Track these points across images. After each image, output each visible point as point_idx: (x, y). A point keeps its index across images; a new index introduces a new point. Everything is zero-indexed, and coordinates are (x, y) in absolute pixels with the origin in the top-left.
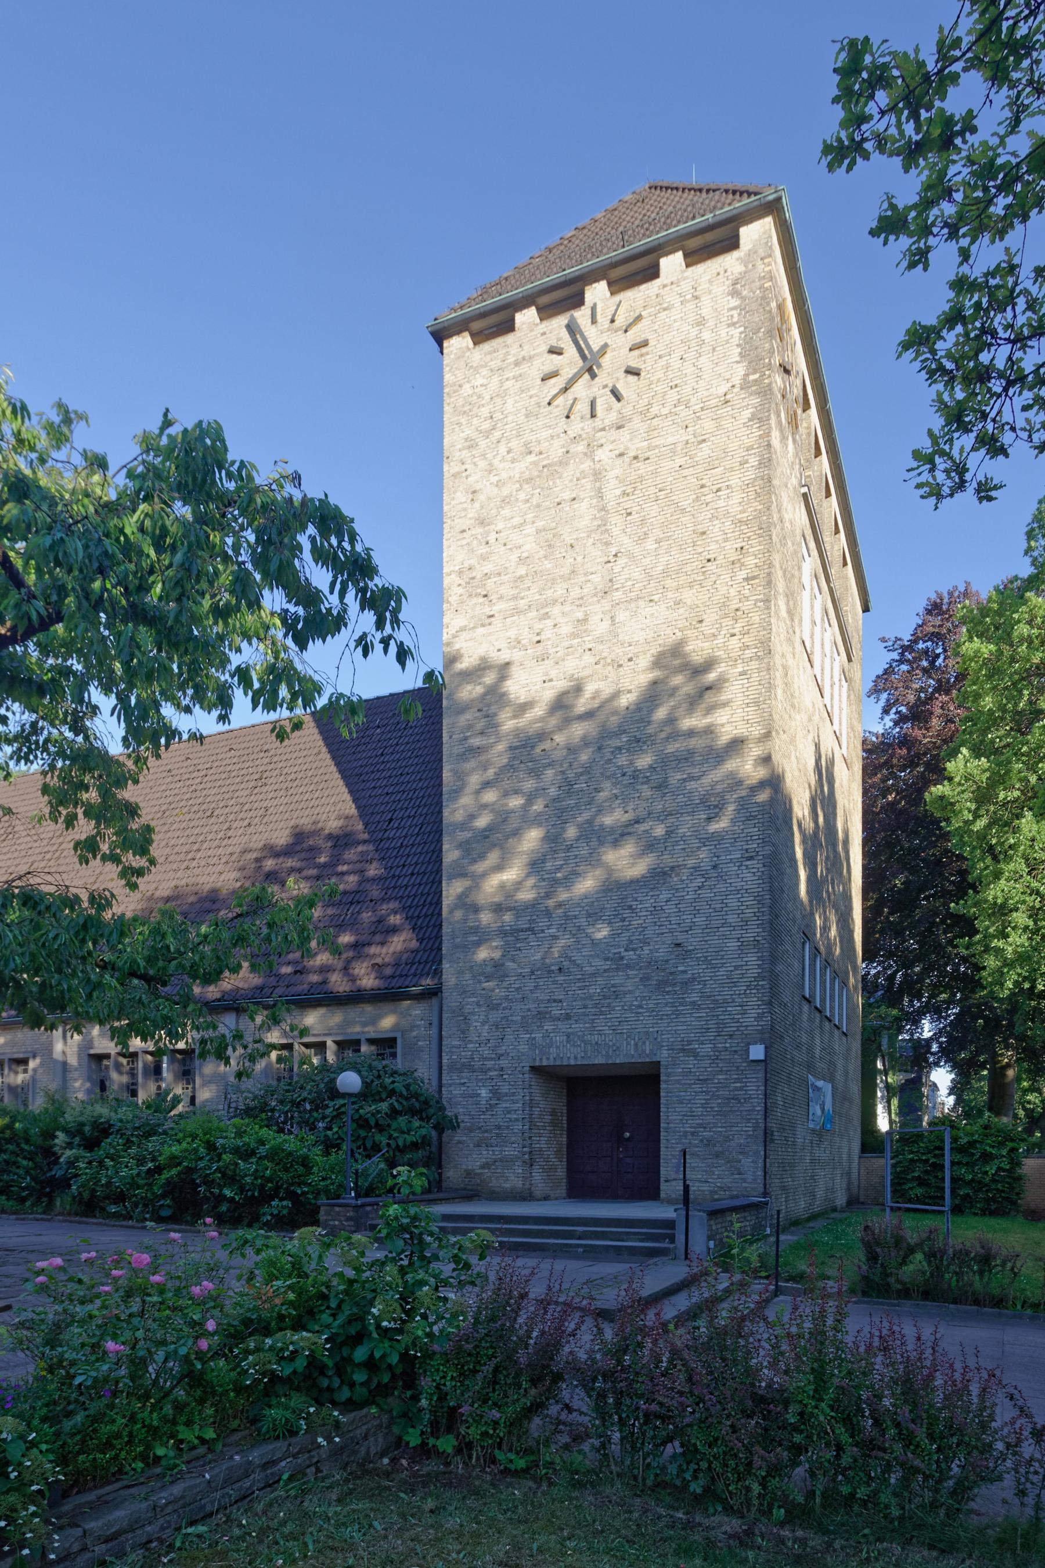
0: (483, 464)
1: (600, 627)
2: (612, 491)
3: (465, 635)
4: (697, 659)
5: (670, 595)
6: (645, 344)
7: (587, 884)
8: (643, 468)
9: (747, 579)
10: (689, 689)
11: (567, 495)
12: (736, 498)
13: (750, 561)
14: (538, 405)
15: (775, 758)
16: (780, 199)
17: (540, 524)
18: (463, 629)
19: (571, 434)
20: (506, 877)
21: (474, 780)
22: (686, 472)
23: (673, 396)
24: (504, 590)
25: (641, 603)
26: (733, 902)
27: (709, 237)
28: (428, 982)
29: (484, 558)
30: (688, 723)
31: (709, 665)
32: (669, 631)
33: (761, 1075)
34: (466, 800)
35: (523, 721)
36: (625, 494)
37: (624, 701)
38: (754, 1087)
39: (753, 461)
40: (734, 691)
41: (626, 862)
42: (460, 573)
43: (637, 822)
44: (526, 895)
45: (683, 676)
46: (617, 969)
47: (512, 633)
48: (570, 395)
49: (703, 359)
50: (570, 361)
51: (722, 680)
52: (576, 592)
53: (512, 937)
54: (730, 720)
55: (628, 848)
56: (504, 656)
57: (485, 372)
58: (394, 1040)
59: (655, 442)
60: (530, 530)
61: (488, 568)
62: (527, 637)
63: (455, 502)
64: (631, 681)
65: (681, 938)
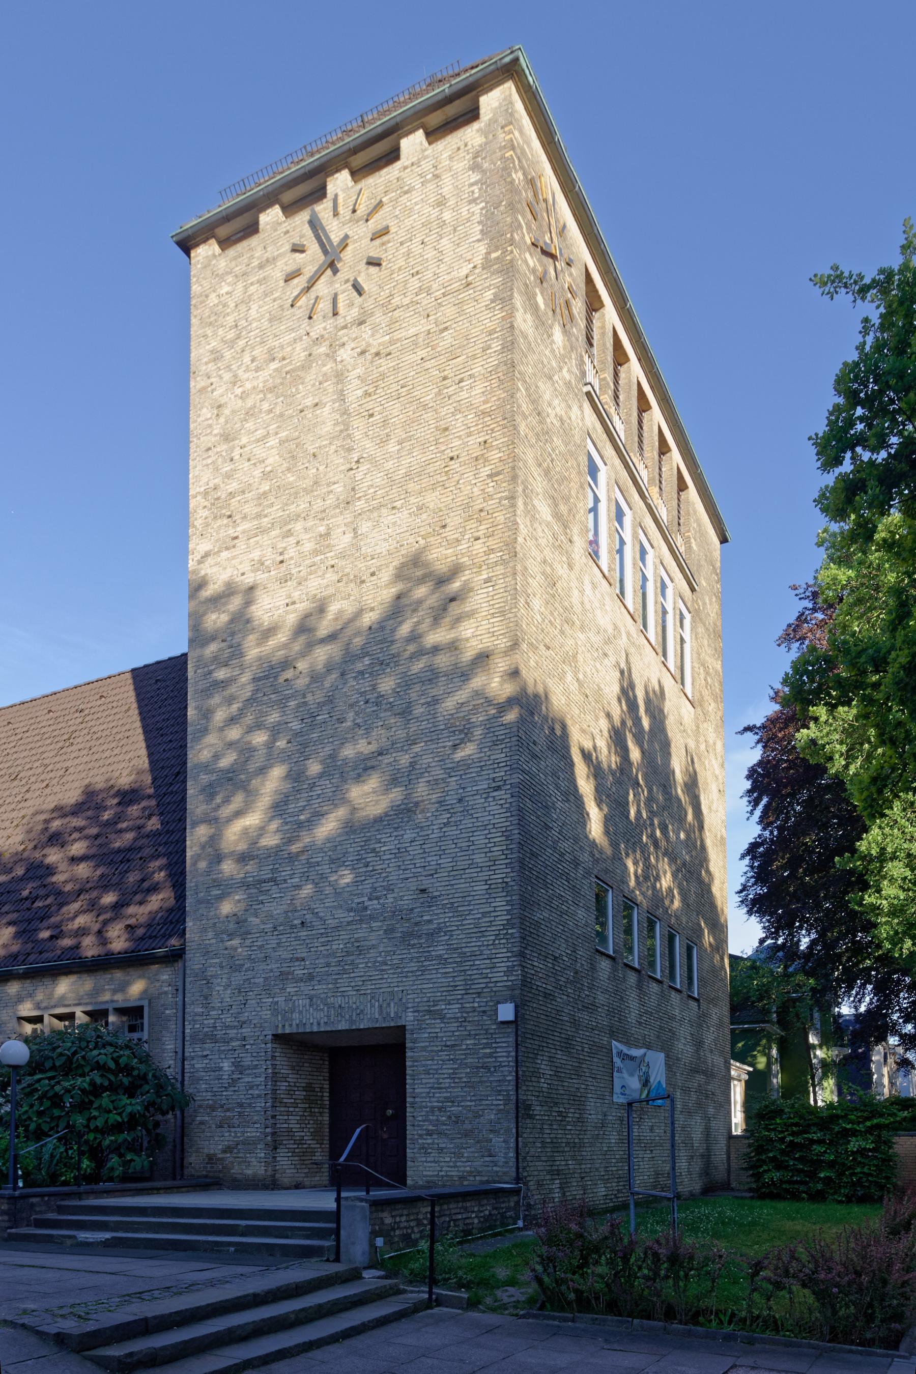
0: (227, 376)
1: (342, 540)
2: (354, 392)
3: (210, 560)
4: (441, 567)
6: (385, 231)
8: (385, 364)
9: (490, 476)
10: (433, 601)
11: (309, 402)
13: (495, 455)
15: (524, 672)
18: (207, 555)
22: (428, 365)
23: (414, 283)
25: (384, 511)
28: (174, 942)
29: (228, 476)
30: (434, 638)
31: (456, 571)
32: (412, 540)
33: (512, 1039)
34: (211, 739)
36: (367, 394)
38: (505, 1053)
39: (496, 346)
41: (369, 797)
44: (270, 841)
45: (431, 586)
47: (256, 555)
48: (312, 294)
49: (444, 241)
50: (314, 255)
53: (255, 888)
54: (476, 632)
55: (373, 783)
56: (249, 579)
57: (230, 279)
59: (397, 335)
60: (273, 441)
61: (233, 486)
62: (271, 557)
64: (377, 596)
65: (426, 883)
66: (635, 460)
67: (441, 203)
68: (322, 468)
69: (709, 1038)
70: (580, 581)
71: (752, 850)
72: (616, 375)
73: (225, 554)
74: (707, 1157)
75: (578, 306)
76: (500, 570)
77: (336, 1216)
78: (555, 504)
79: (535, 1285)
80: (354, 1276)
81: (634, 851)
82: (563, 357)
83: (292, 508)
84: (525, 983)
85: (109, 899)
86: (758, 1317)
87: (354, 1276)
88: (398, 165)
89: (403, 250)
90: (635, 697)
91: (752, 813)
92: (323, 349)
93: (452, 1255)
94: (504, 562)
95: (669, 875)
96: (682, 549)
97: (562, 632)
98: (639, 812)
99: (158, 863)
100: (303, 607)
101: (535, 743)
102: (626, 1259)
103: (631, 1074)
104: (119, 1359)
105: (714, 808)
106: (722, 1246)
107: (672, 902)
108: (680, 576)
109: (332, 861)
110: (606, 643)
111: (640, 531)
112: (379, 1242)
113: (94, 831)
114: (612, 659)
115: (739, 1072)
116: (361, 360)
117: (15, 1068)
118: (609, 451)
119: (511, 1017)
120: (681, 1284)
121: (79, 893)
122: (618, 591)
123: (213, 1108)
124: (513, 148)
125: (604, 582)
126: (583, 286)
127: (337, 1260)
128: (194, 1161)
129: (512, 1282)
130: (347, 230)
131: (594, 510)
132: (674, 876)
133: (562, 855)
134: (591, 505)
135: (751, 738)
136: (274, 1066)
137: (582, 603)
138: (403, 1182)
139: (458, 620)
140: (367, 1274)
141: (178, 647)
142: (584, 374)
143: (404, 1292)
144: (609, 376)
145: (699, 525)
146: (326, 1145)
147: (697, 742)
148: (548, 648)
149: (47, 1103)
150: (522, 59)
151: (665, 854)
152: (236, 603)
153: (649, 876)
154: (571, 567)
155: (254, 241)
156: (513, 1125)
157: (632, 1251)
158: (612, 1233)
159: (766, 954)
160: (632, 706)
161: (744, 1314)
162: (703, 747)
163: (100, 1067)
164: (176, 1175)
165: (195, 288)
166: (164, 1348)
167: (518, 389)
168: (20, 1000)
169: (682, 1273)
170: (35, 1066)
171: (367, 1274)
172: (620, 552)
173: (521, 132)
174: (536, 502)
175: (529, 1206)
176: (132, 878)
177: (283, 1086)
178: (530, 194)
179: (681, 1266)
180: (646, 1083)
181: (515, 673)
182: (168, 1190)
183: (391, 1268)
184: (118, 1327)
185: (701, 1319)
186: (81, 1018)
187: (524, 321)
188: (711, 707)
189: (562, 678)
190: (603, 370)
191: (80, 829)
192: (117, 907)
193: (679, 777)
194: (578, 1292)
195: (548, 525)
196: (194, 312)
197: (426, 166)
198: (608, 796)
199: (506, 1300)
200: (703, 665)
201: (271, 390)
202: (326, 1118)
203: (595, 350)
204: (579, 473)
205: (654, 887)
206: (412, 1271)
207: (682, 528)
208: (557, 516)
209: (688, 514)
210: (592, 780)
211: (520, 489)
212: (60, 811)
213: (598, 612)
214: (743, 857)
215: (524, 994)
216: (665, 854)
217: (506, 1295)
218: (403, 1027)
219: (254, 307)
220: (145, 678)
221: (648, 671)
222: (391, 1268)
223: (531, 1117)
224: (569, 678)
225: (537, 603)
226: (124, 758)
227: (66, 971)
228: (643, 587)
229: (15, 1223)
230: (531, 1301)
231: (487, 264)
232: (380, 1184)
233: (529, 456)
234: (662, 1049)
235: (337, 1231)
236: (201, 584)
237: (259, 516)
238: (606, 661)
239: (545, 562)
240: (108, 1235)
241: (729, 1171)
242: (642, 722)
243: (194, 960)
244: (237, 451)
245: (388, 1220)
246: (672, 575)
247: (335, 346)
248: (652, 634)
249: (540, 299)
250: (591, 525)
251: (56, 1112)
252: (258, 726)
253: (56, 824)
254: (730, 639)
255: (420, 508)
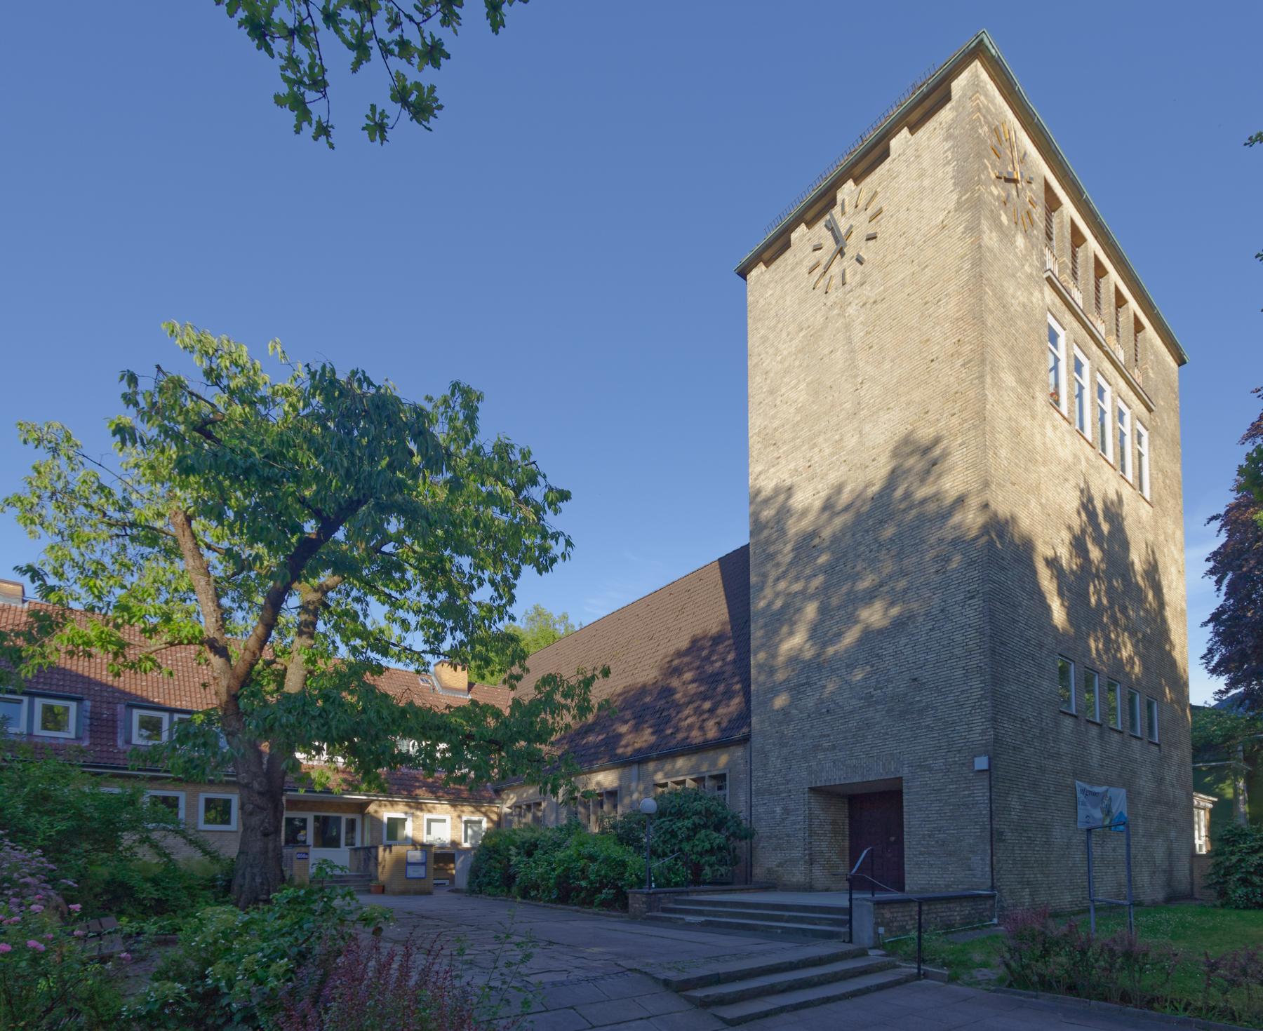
0: (771, 351)
1: (851, 441)
2: (858, 334)
3: (762, 477)
4: (926, 442)
5: (903, 399)
6: (880, 212)
7: (851, 637)
8: (880, 307)
9: (963, 365)
10: (920, 466)
11: (826, 351)
12: (953, 302)
13: (967, 348)
14: (807, 292)
15: (993, 506)
16: (982, 40)
17: (809, 379)
18: (760, 473)
19: (829, 304)
20: (795, 642)
21: (773, 574)
22: (912, 298)
23: (903, 241)
24: (787, 436)
25: (881, 413)
26: (958, 637)
27: (928, 104)
28: (745, 730)
29: (774, 417)
30: (921, 493)
31: (937, 441)
32: (902, 428)
33: (986, 783)
34: (768, 592)
35: (804, 523)
36: (868, 333)
37: (875, 489)
38: (980, 793)
39: (967, 266)
40: (958, 458)
41: (874, 615)
42: (759, 432)
43: (881, 586)
44: (808, 654)
45: (920, 456)
46: (869, 706)
47: (792, 466)
48: (828, 276)
49: (925, 202)
50: (829, 244)
51: (945, 455)
52: (508, 979)
53: (797, 690)
54: (952, 483)
55: (878, 605)
56: (788, 483)
57: (772, 285)
58: (724, 775)
59: (889, 284)
60: (802, 386)
61: (777, 423)
62: (802, 464)
63: (756, 383)
64: (878, 472)
65: (917, 674)
66: (1092, 319)
67: (921, 176)
68: (836, 395)
69: (1170, 775)
70: (1042, 426)
71: (1215, 618)
72: (1074, 256)
73: (772, 470)
74: (1170, 872)
75: (1038, 213)
76: (972, 433)
77: (849, 911)
78: (1018, 371)
79: (1003, 967)
80: (862, 953)
81: (1095, 631)
82: (1025, 257)
83: (817, 428)
84: (997, 740)
85: (707, 705)
86: (1214, 1008)
87: (862, 953)
88: (889, 159)
89: (893, 220)
90: (1094, 507)
91: (1218, 590)
92: (836, 312)
93: (935, 942)
94: (975, 427)
95: (1129, 645)
96: (1140, 381)
97: (1026, 470)
98: (1099, 600)
99: (736, 679)
100: (824, 494)
101: (1003, 559)
102: (1084, 952)
103: (1095, 807)
104: (700, 999)
105: (1174, 586)
106: (1180, 947)
107: (1132, 667)
108: (1138, 402)
109: (848, 666)
110: (1066, 470)
111: (1098, 375)
112: (881, 930)
113: (697, 663)
114: (1072, 482)
115: (1203, 803)
116: (864, 310)
117: (649, 815)
118: (1068, 318)
119: (985, 767)
120: (1137, 975)
121: (690, 703)
122: (1077, 427)
123: (770, 838)
124: (979, 110)
125: (1065, 423)
126: (1042, 195)
127: (851, 941)
128: (759, 872)
129: (985, 965)
130: (852, 222)
131: (1055, 369)
132: (1135, 646)
133: (1028, 640)
134: (1052, 364)
135: (1217, 524)
136: (810, 809)
137: (1044, 444)
138: (901, 888)
139: (940, 476)
140: (871, 953)
141: (743, 540)
142: (1044, 264)
143: (899, 967)
144: (1067, 259)
145: (1156, 356)
146: (847, 859)
147: (1156, 535)
148: (1014, 484)
149: (668, 836)
150: (986, 40)
151: (1126, 629)
152: (782, 497)
153: (1111, 646)
154: (1033, 417)
155: (788, 254)
156: (988, 847)
157: (1090, 946)
158: (1070, 931)
159: (1225, 705)
160: (1092, 515)
161: (1199, 1004)
162: (1162, 538)
163: (697, 813)
164: (747, 881)
165: (750, 299)
166: (729, 994)
167: (986, 293)
168: (655, 772)
169: (1137, 968)
170: (661, 813)
171: (871, 953)
172: (1080, 396)
173: (986, 96)
174: (1002, 375)
175: (1003, 908)
176: (721, 688)
177: (816, 822)
178: (994, 140)
179: (1136, 961)
180: (1108, 812)
181: (986, 506)
182: (742, 890)
183: (892, 950)
184: (701, 978)
185: (1156, 1005)
186: (690, 784)
187: (990, 239)
188: (1170, 504)
189: (1026, 505)
190: (1061, 256)
191: (688, 664)
192: (712, 711)
193: (1138, 567)
194: (1041, 976)
195: (1013, 389)
196: (749, 315)
197: (910, 152)
198: (1069, 590)
199: (980, 978)
200: (1161, 471)
201: (800, 351)
202: (847, 844)
203: (1054, 243)
204: (1041, 343)
205: (1115, 657)
206: (906, 953)
207: (1139, 363)
208: (1021, 381)
209: (1146, 349)
210: (1055, 581)
211: (988, 368)
212: (679, 654)
213: (1059, 448)
214: (1205, 624)
215: (995, 749)
216: (1124, 630)
217: (979, 974)
218: (901, 778)
219: (788, 298)
220: (725, 562)
221: (1106, 485)
222: (891, 949)
223: (1004, 841)
224: (1033, 503)
225: (1003, 452)
226: (713, 614)
227: (682, 754)
228: (1102, 420)
229: (650, 909)
230: (1001, 980)
231: (959, 206)
232: (882, 890)
233: (995, 341)
234: (1123, 786)
235: (850, 921)
236: (758, 492)
237: (794, 439)
238: (1067, 485)
239: (1010, 419)
240: (703, 919)
241: (1192, 884)
242: (1103, 527)
243: (756, 742)
244: (779, 399)
245: (888, 915)
246: (1129, 402)
247: (843, 305)
248: (1110, 456)
249: (1004, 219)
250: (1052, 381)
251: (673, 841)
252: (797, 579)
253: (676, 662)
254: (1190, 446)
255: (908, 404)
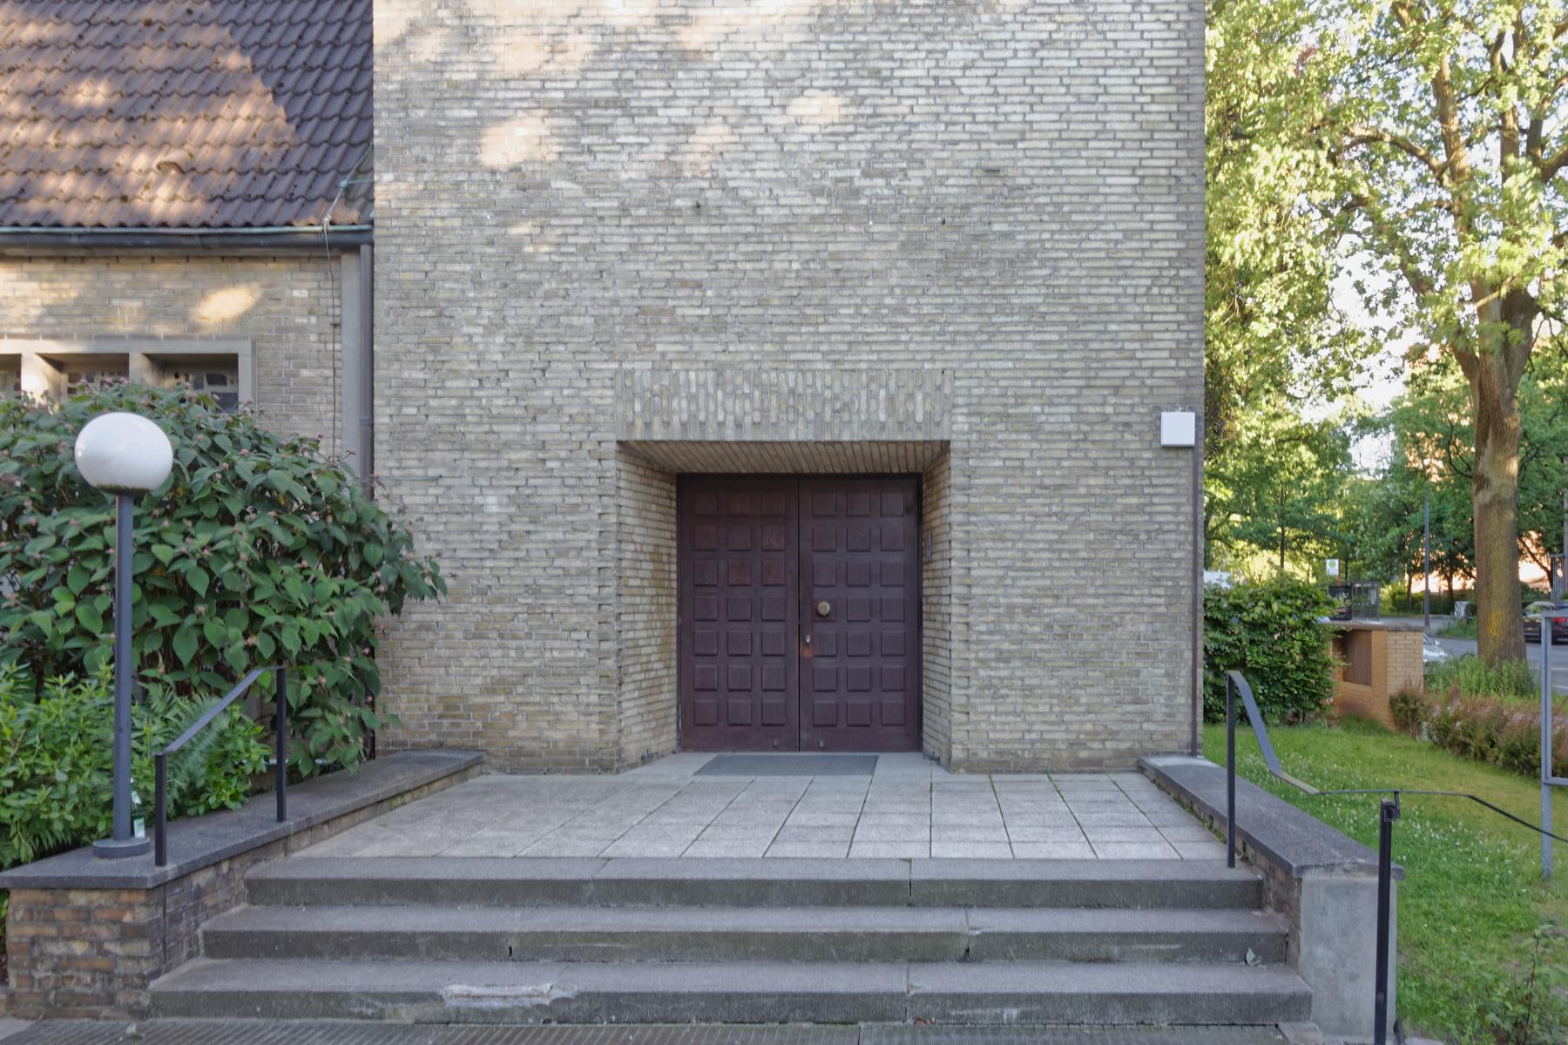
26: (1120, 85)
28: (349, 216)
46: (845, 218)
109: (772, 83)
218: (945, 446)
